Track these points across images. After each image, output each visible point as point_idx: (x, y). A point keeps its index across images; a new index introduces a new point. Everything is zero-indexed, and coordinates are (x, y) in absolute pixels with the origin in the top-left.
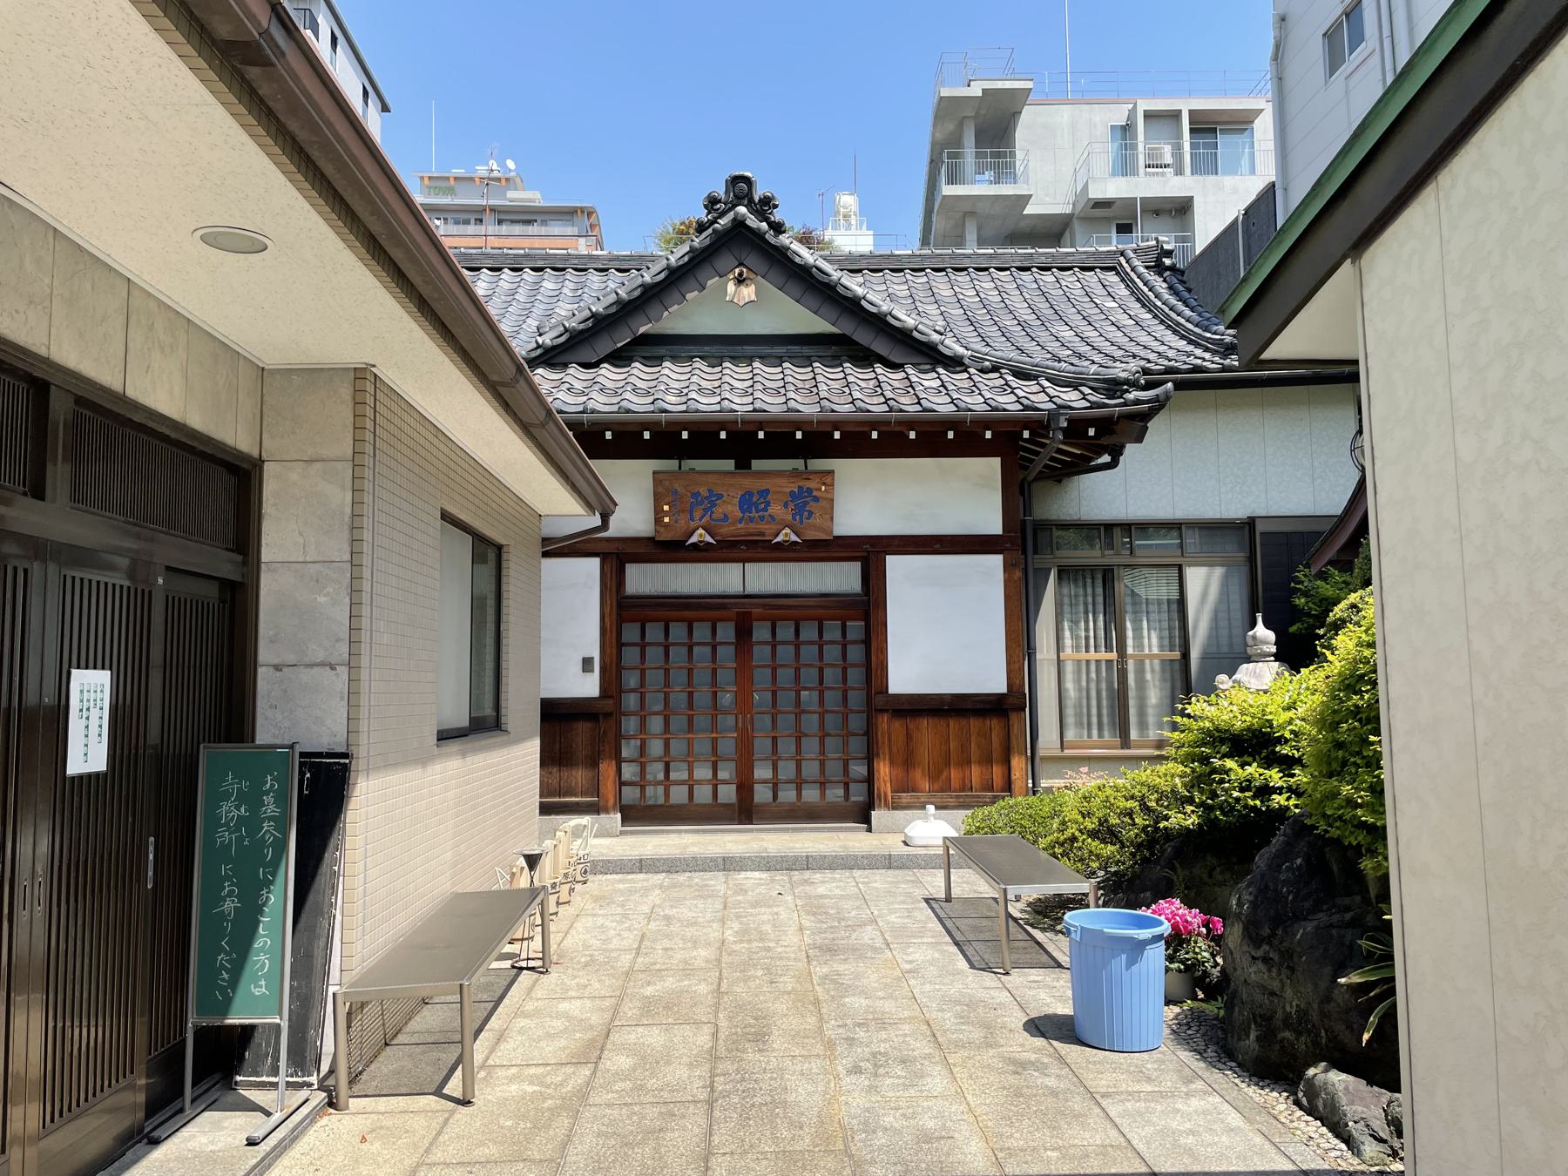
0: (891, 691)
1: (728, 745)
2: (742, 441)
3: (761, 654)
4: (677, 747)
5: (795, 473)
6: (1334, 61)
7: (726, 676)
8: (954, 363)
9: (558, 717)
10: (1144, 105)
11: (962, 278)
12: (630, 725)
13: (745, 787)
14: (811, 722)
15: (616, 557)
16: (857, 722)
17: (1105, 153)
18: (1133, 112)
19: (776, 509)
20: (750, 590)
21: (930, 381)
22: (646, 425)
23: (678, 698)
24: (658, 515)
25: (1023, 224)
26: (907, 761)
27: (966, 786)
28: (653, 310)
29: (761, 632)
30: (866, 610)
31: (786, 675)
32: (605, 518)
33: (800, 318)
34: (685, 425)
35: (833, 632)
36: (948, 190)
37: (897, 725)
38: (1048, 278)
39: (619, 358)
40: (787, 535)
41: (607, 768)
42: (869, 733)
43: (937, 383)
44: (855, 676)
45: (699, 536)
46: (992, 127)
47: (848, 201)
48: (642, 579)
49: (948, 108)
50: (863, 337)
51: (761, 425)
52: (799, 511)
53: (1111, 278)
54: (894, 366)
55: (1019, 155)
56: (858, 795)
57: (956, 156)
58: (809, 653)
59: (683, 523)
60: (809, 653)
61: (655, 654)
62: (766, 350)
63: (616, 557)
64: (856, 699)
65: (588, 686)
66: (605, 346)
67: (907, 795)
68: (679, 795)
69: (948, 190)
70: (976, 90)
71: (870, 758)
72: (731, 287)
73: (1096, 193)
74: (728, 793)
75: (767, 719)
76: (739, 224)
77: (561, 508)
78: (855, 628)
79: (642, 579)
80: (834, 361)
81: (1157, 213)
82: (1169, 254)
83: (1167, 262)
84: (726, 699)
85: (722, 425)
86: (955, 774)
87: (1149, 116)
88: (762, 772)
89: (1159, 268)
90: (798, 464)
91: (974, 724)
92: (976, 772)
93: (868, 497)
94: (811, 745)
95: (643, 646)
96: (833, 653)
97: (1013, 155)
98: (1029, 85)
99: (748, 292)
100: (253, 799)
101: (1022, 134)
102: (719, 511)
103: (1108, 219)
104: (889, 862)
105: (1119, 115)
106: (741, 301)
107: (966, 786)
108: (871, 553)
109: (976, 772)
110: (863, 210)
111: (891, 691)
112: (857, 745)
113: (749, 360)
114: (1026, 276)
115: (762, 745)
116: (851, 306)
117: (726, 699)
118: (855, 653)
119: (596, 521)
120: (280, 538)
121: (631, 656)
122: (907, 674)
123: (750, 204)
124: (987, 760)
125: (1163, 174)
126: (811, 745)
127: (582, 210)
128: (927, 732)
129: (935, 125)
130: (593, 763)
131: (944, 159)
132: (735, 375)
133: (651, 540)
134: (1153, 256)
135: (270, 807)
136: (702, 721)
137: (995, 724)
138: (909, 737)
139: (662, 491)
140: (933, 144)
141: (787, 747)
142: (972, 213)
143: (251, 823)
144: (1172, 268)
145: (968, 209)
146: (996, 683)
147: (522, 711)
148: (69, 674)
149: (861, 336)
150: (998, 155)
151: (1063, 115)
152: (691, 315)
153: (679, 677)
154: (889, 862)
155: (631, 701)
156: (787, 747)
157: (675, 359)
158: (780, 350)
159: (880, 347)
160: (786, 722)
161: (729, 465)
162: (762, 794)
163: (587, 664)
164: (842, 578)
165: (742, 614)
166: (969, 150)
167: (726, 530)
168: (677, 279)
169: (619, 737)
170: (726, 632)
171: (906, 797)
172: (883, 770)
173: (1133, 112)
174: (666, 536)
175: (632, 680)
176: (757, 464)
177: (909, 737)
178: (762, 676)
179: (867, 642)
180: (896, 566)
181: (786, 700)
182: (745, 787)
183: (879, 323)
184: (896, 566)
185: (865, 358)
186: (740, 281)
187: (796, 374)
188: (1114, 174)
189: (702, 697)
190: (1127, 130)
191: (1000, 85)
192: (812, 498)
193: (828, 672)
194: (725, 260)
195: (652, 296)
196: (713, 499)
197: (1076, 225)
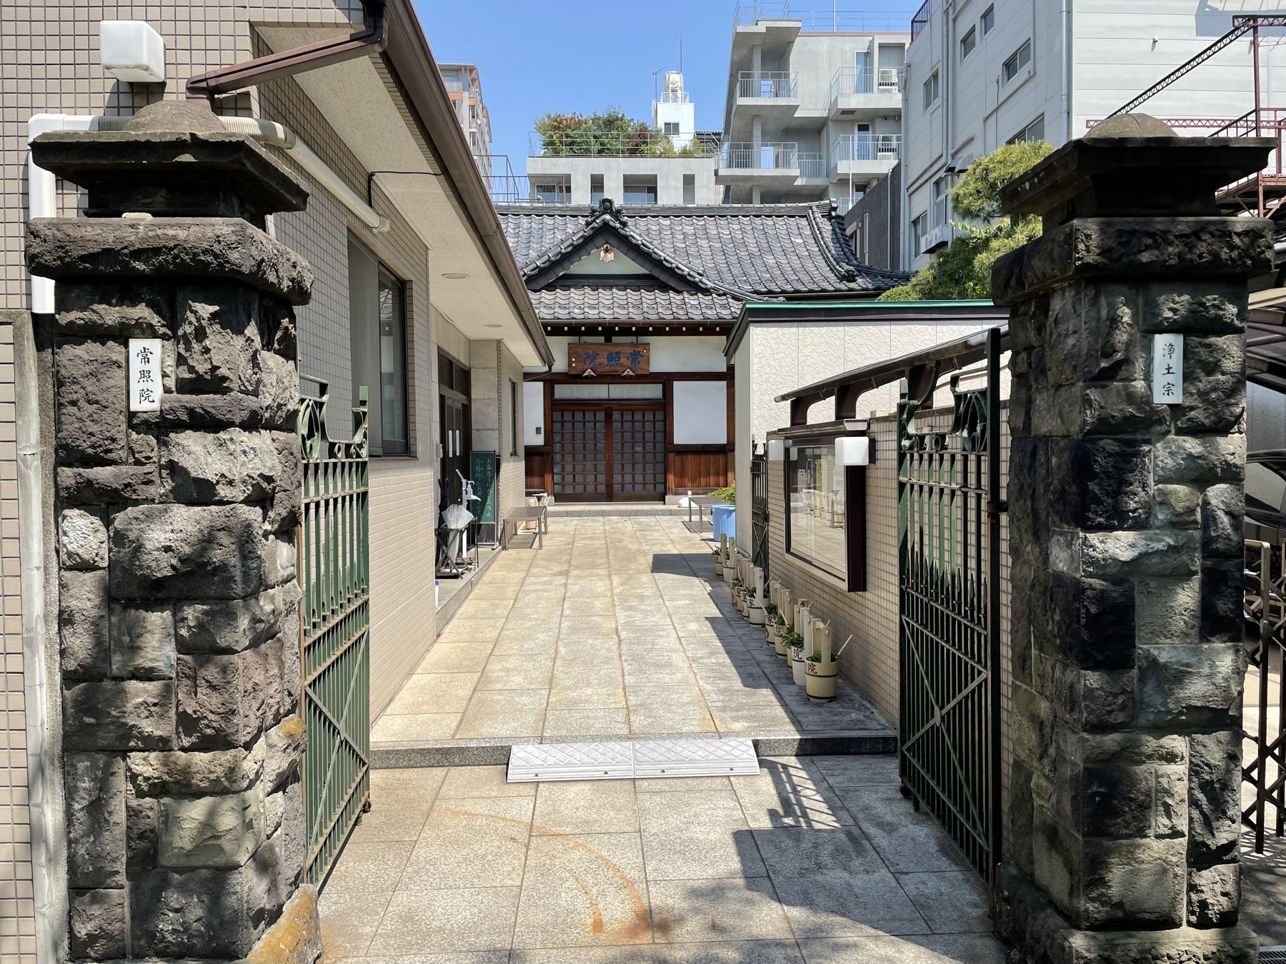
0: (676, 442)
1: (602, 466)
2: (608, 330)
3: (616, 426)
4: (579, 468)
5: (632, 344)
6: (928, 103)
7: (600, 436)
8: (706, 291)
9: (531, 452)
10: (878, 40)
11: (723, 222)
12: (558, 457)
13: (609, 486)
14: (639, 457)
15: (550, 381)
16: (660, 457)
17: (852, 72)
18: (872, 42)
19: (623, 360)
20: (612, 396)
21: (692, 300)
22: (566, 325)
23: (579, 446)
24: (570, 365)
25: (794, 123)
26: (681, 474)
27: (708, 485)
28: (566, 264)
29: (616, 416)
30: (664, 406)
31: (628, 436)
32: (550, 367)
33: (631, 267)
34: (583, 325)
35: (649, 416)
36: (741, 101)
37: (678, 458)
38: (769, 222)
39: (550, 287)
40: (628, 372)
41: (548, 477)
42: (665, 462)
43: (696, 302)
44: (659, 437)
45: (589, 372)
46: (773, 53)
47: (675, 78)
48: (563, 391)
49: (741, 40)
50: (664, 278)
51: (617, 325)
52: (634, 361)
53: (804, 222)
54: (678, 292)
55: (792, 77)
56: (660, 488)
57: (749, 76)
58: (638, 425)
59: (581, 367)
60: (638, 425)
61: (568, 426)
62: (619, 282)
63: (550, 381)
64: (660, 447)
65: (539, 440)
66: (543, 282)
67: (680, 490)
68: (580, 489)
69: (741, 101)
70: (761, 28)
71: (665, 473)
72: (602, 254)
73: (844, 104)
74: (602, 488)
75: (619, 456)
76: (606, 224)
77: (533, 362)
78: (659, 415)
79: (563, 391)
80: (650, 289)
81: (886, 118)
82: (835, 209)
83: (833, 214)
84: (600, 446)
85: (600, 324)
86: (703, 480)
87: (881, 46)
88: (617, 478)
89: (830, 218)
90: (633, 339)
91: (712, 457)
92: (712, 480)
93: (665, 355)
94: (639, 467)
95: (563, 422)
96: (648, 426)
97: (787, 76)
98: (798, 24)
99: (610, 256)
100: (484, 465)
101: (794, 58)
102: (597, 361)
103: (853, 122)
104: (671, 513)
105: (861, 45)
106: (607, 260)
107: (708, 485)
108: (666, 380)
109: (712, 480)
110: (687, 86)
111: (676, 442)
112: (660, 467)
113: (611, 287)
114: (758, 220)
115: (617, 467)
116: (659, 263)
117: (600, 446)
118: (659, 426)
119: (547, 369)
120: (476, 392)
121: (557, 427)
122: (681, 436)
123: (611, 213)
124: (717, 474)
125: (890, 91)
126: (639, 467)
127: (466, 68)
128: (691, 461)
129: (733, 50)
130: (542, 475)
131: (740, 76)
132: (605, 295)
133: (566, 374)
134: (827, 210)
135: (489, 468)
136: (589, 456)
137: (721, 458)
138: (682, 463)
139: (572, 352)
140: (733, 64)
141: (628, 468)
142: (758, 116)
143: (485, 471)
144: (838, 217)
145: (755, 114)
146: (723, 440)
147: (521, 452)
148: (813, 426)
149: (660, 275)
150: (779, 76)
151: (823, 44)
152: (584, 266)
153: (579, 436)
154: (671, 513)
155: (557, 447)
156: (628, 468)
157: (576, 287)
158: (625, 282)
159: (672, 283)
160: (628, 457)
161: (601, 339)
162: (617, 488)
163: (538, 430)
164: (653, 391)
165: (608, 407)
166: (757, 72)
167: (600, 370)
168: (578, 249)
169: (552, 464)
170: (601, 416)
171: (681, 490)
172: (671, 478)
173: (872, 42)
174: (573, 372)
175: (557, 438)
176: (615, 339)
177: (682, 463)
178: (617, 436)
179: (665, 421)
180: (678, 386)
181: (628, 447)
182: (609, 486)
183: (672, 272)
184: (678, 386)
185: (665, 288)
186: (606, 251)
187: (632, 295)
188: (857, 91)
189: (590, 446)
190: (868, 55)
191: (778, 24)
192: (640, 355)
193: (647, 435)
194: (600, 241)
195: (565, 258)
196: (595, 355)
197: (830, 123)
